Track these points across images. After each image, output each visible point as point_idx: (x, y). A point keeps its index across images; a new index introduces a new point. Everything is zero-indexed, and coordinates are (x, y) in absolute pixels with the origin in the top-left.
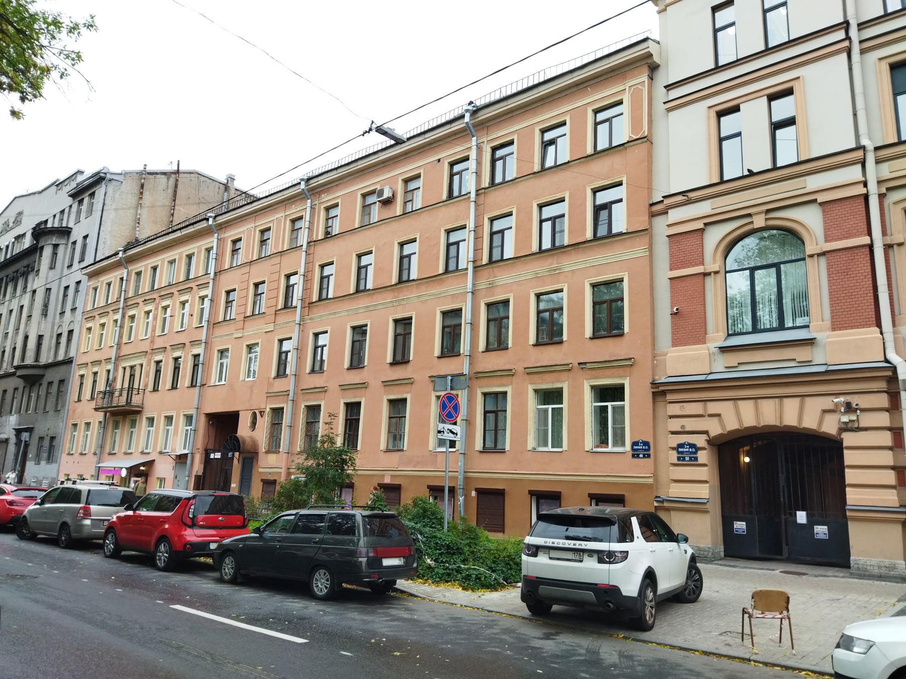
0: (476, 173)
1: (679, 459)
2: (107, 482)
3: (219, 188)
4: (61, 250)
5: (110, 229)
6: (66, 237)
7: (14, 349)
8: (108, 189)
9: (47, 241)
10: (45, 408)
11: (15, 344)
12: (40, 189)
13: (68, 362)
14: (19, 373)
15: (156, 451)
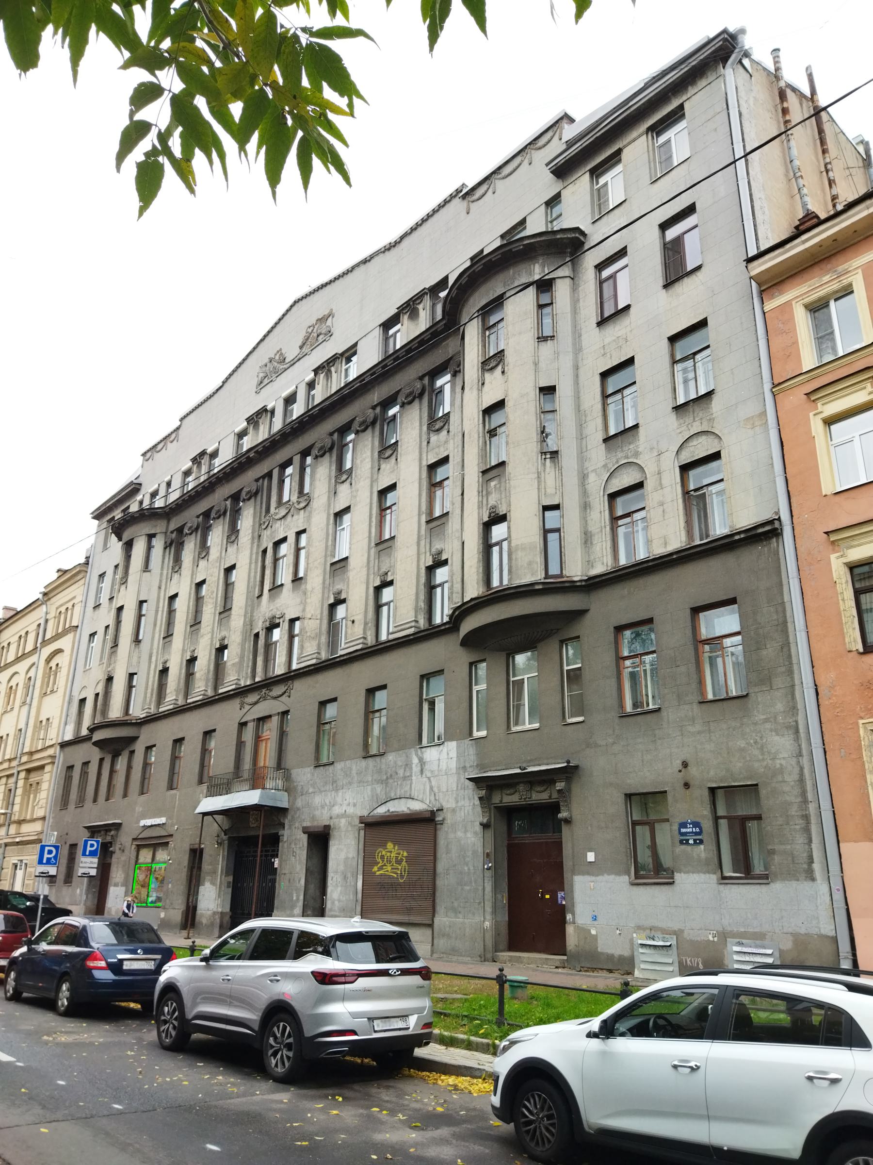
11: (165, 662)
14: (98, 736)
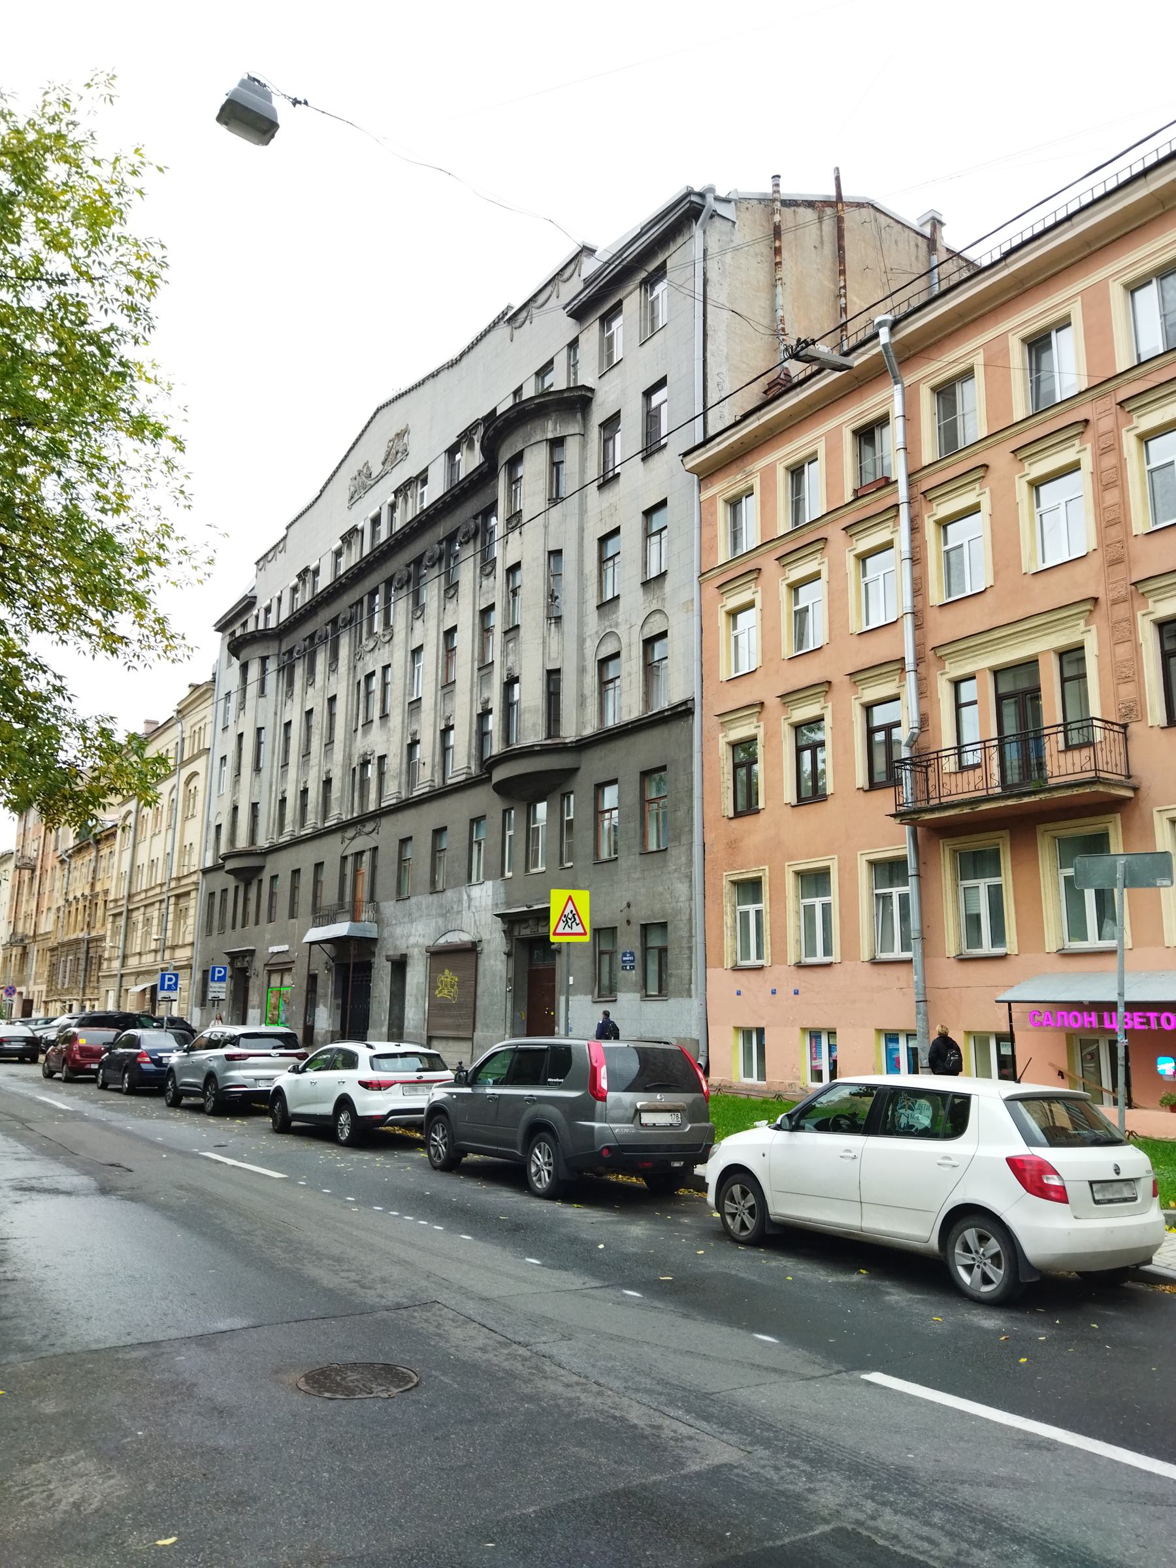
0: (905, 449)
3: (917, 246)
4: (572, 448)
5: (725, 350)
6: (579, 416)
7: (305, 792)
8: (709, 240)
9: (530, 436)
11: (284, 792)
12: (455, 354)
13: (682, 712)
14: (230, 865)
15: (785, 962)
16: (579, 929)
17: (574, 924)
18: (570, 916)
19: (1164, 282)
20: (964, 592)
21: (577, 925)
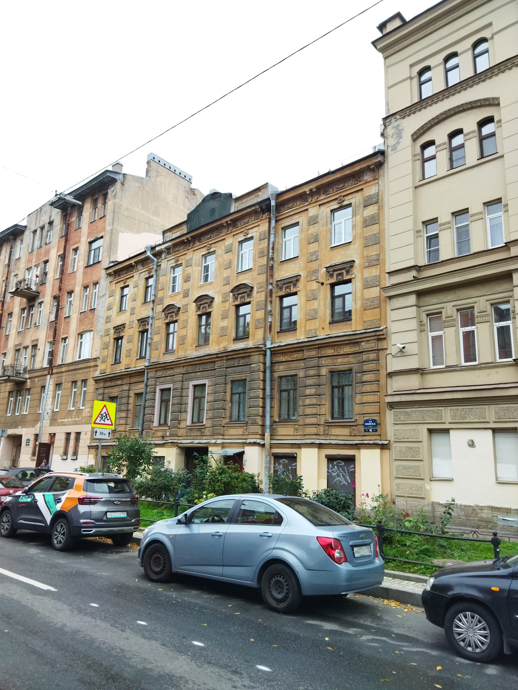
1: (365, 431)
2: (372, 179)
10: (354, 422)
16: (109, 422)
17: (106, 419)
18: (104, 415)
19: (457, 217)
20: (341, 241)
21: (108, 420)
